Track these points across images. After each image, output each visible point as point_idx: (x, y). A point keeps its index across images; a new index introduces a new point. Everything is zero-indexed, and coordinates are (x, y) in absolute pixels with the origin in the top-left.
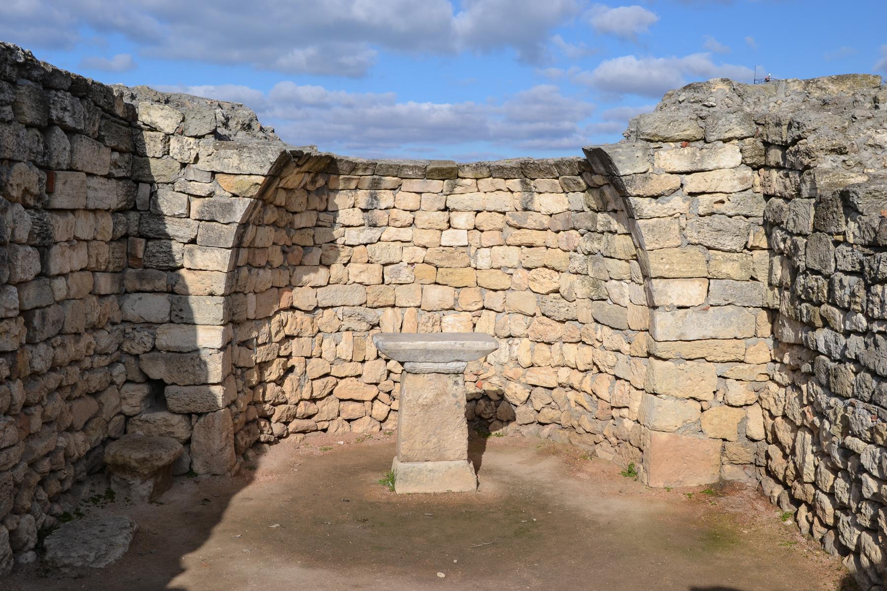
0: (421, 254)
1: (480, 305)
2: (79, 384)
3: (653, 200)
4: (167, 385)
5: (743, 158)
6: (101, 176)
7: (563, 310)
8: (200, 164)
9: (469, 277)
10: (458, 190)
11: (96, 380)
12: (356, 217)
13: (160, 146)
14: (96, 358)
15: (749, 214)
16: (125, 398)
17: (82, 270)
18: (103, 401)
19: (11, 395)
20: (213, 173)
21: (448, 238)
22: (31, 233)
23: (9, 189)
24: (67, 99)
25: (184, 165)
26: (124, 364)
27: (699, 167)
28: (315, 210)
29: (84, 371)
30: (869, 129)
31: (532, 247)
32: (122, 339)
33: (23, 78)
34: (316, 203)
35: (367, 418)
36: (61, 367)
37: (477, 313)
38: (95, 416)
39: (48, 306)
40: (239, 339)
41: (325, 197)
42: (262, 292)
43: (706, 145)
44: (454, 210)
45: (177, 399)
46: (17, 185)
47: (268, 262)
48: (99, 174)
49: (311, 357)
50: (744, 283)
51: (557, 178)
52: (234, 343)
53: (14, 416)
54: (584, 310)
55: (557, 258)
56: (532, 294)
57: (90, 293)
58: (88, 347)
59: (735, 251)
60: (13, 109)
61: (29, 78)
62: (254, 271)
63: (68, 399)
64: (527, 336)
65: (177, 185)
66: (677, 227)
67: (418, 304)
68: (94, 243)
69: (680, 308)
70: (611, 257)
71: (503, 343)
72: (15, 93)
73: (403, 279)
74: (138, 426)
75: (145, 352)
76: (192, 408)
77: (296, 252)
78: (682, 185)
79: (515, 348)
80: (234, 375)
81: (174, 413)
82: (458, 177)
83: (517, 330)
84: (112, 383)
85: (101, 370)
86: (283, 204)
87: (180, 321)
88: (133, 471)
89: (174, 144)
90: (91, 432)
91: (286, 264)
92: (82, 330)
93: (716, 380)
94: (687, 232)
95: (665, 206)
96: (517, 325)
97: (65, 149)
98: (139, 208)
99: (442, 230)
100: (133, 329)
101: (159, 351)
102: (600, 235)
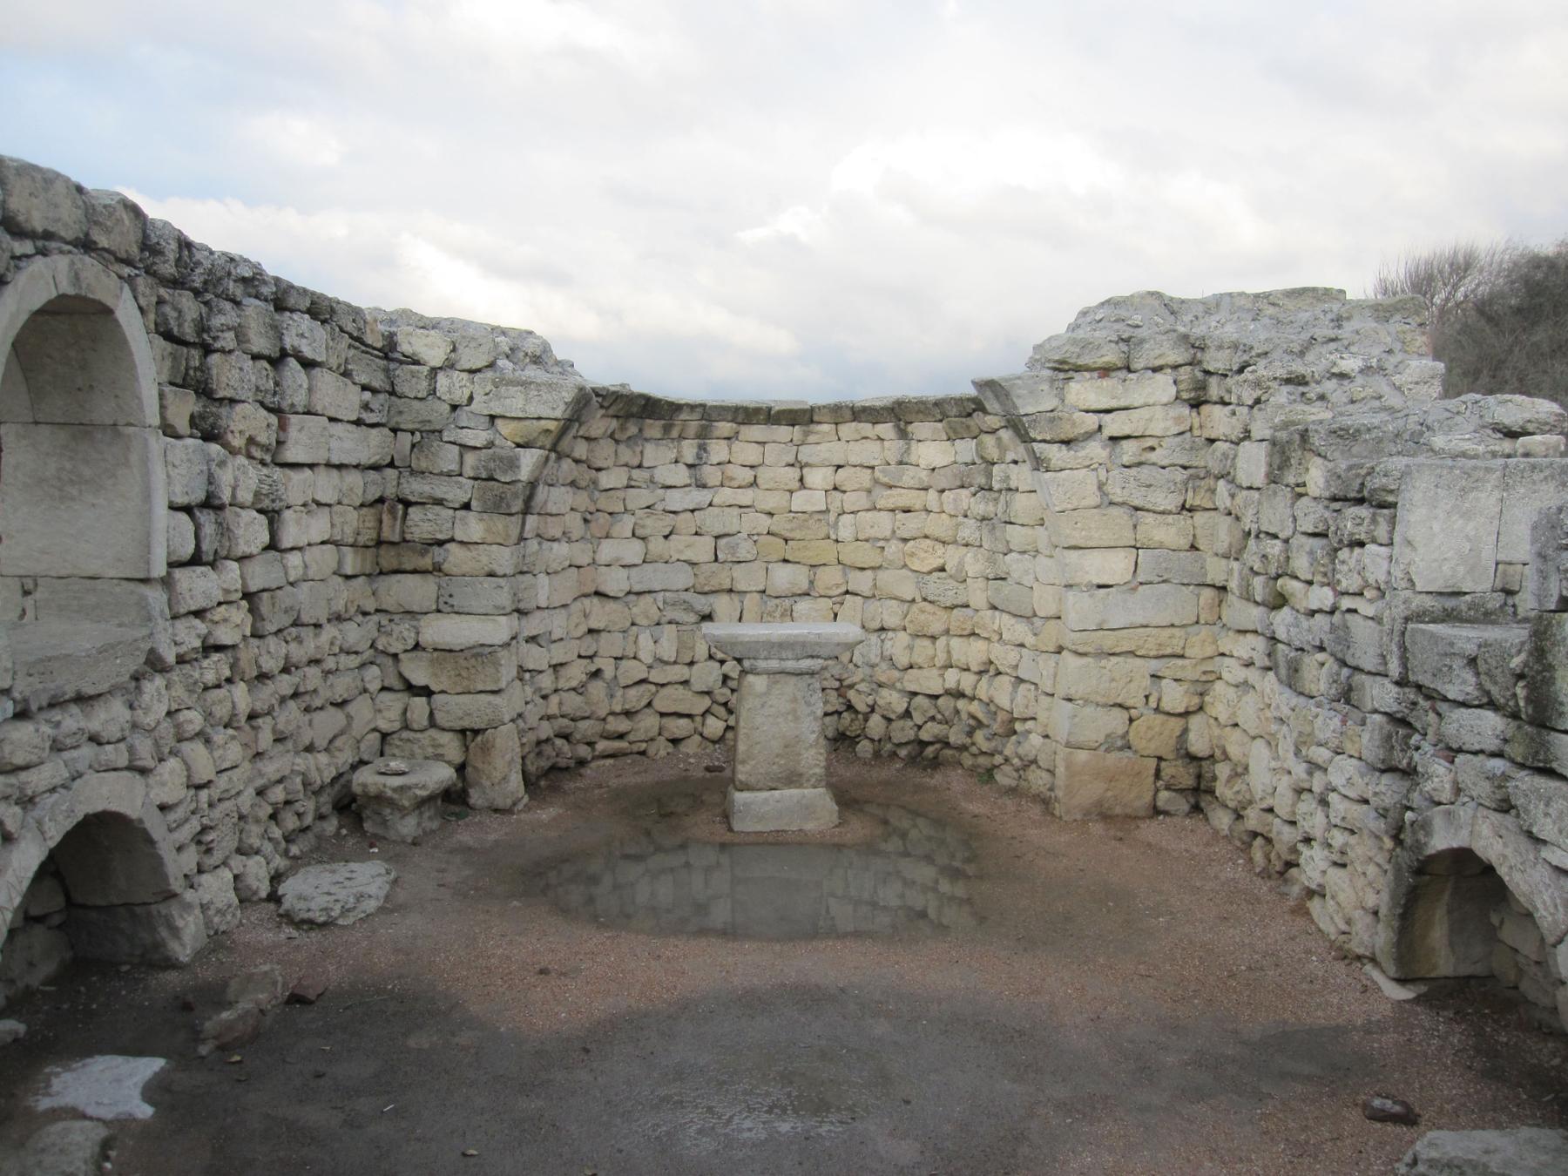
0: (764, 523)
1: (843, 589)
2: (321, 691)
3: (1064, 447)
4: (433, 693)
5: (1178, 392)
6: (348, 422)
7: (951, 593)
8: (474, 406)
9: (827, 552)
10: (811, 439)
11: (341, 686)
12: (681, 475)
13: (425, 384)
14: (343, 657)
15: (1187, 464)
16: (380, 711)
17: (323, 543)
18: (352, 714)
19: (233, 703)
20: (492, 418)
21: (800, 501)
22: (257, 494)
23: (230, 437)
24: (305, 322)
25: (454, 408)
26: (378, 665)
27: (1122, 403)
28: (626, 465)
29: (327, 673)
30: (1331, 353)
31: (909, 511)
32: (376, 634)
33: (250, 296)
34: (626, 454)
35: (697, 738)
36: (297, 668)
37: (839, 599)
38: (342, 733)
39: (280, 588)
40: (527, 633)
41: (638, 449)
42: (556, 572)
43: (1131, 376)
44: (807, 465)
45: (448, 712)
46: (240, 432)
47: (564, 533)
48: (345, 419)
49: (621, 659)
50: (1182, 554)
51: (941, 421)
52: (520, 638)
53: (236, 729)
54: (977, 594)
55: (938, 525)
56: (910, 573)
57: (335, 573)
58: (332, 644)
59: (1170, 513)
60: (237, 336)
61: (257, 297)
62: (546, 545)
63: (307, 710)
64: (905, 629)
65: (445, 433)
66: (1095, 482)
67: (761, 588)
68: (337, 508)
69: (1100, 586)
70: (1011, 523)
71: (874, 638)
72: (239, 316)
73: (742, 555)
74: (398, 747)
75: (406, 651)
76: (466, 723)
77: (601, 521)
78: (1100, 427)
79: (888, 644)
80: (521, 680)
81: (443, 729)
82: (812, 422)
83: (891, 622)
84: (365, 691)
85: (349, 673)
86: (584, 458)
87: (449, 609)
88: (391, 803)
89: (442, 380)
90: (337, 753)
91: (589, 536)
92: (323, 621)
93: (1147, 681)
94: (1108, 488)
95: (1080, 454)
96: (890, 614)
97: (301, 386)
98: (396, 463)
99: (791, 492)
100: (391, 621)
101: (424, 649)
102: (996, 495)
